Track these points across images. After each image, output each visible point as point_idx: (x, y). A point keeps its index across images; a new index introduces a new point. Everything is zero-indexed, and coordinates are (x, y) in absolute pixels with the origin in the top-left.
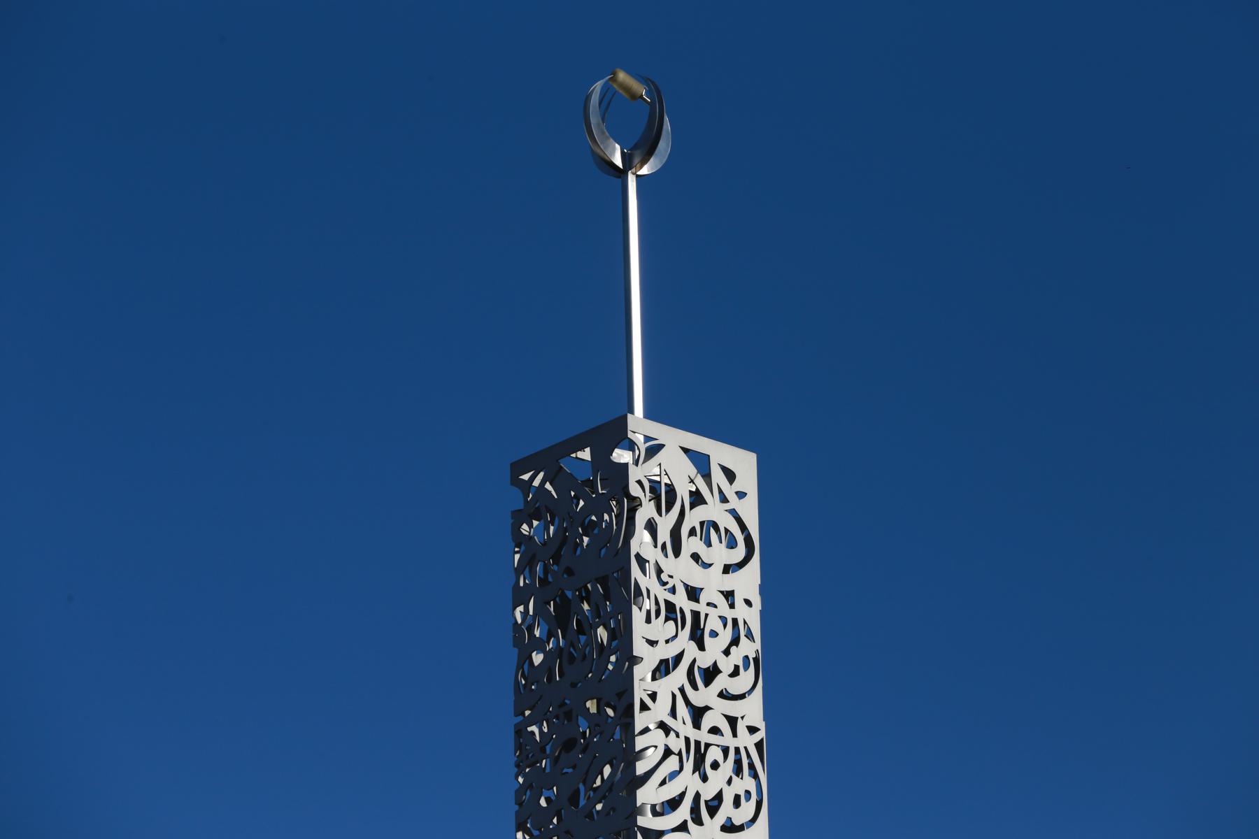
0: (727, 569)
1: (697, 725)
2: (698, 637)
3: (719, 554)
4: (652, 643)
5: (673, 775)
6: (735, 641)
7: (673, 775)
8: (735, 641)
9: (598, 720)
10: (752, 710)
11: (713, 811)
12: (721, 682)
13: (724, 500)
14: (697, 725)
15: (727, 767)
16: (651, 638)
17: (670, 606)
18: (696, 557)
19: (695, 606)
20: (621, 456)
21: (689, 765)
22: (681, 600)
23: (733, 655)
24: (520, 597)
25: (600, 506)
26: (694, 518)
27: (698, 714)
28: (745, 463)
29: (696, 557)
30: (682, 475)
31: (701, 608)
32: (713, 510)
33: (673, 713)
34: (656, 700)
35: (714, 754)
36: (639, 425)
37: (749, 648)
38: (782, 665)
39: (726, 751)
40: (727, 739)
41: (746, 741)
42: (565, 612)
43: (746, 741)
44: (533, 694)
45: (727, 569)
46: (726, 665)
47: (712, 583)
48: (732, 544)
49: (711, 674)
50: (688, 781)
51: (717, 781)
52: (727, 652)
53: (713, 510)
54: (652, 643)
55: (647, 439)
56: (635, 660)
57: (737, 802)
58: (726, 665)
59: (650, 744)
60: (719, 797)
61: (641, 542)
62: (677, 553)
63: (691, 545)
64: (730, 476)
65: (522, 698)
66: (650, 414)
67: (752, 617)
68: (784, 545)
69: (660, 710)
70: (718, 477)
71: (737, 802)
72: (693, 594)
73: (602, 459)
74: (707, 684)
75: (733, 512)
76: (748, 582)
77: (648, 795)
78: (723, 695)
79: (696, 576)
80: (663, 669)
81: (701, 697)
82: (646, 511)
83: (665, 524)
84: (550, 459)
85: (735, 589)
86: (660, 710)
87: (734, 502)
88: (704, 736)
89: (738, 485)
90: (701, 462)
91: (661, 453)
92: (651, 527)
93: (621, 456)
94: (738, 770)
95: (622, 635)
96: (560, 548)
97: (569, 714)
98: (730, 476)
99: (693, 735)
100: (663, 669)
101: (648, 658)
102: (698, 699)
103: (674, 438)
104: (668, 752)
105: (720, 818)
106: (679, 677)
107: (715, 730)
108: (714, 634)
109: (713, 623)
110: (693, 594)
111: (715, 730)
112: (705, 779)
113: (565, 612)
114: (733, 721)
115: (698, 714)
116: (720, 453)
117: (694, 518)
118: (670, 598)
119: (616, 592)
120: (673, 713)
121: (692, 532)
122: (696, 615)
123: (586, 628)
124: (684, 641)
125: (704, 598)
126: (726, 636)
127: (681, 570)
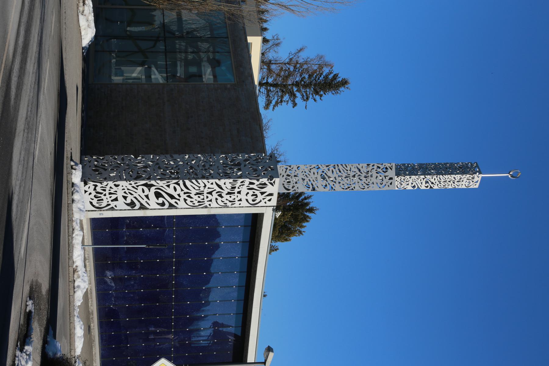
0: (247, 200)
1: (207, 193)
2: (229, 193)
3: (467, 184)
4: (225, 184)
5: (194, 188)
6: (230, 201)
7: (194, 188)
8: (230, 201)
9: (449, 171)
10: (450, 187)
11: (219, 195)
12: (219, 198)
13: (263, 199)
14: (207, 193)
15: (199, 200)
16: (458, 177)
17: (235, 188)
18: (248, 193)
19: (236, 193)
20: (478, 174)
21: (198, 191)
22: (236, 190)
23: (456, 185)
24: (462, 163)
25: (472, 171)
26: (471, 181)
27: (450, 181)
28: (477, 186)
29: (248, 193)
30: (475, 180)
31: (236, 194)
32: (260, 197)
33: (209, 188)
34: (452, 177)
35: (202, 197)
36: (481, 176)
37: (457, 187)
38: (455, 190)
39: (203, 199)
40: (206, 200)
41: (447, 186)
42: (461, 168)
43: (447, 186)
44: (452, 165)
45: (247, 200)
46: (223, 199)
47: (464, 183)
48: (253, 201)
49: (454, 183)
50: (442, 180)
51: (442, 183)
52: (227, 200)
53: (472, 183)
54: (225, 184)
55: (274, 182)
56: (219, 180)
57: (191, 202)
58: (223, 199)
59: (446, 177)
60: (191, 198)
61: (468, 176)
62: (248, 189)
63: (468, 181)
64: (270, 200)
65: (451, 163)
66: (482, 177)
67: (460, 187)
68: (468, 191)
69: (450, 178)
70: (269, 198)
71: (191, 202)
72: (239, 192)
73: (477, 172)
74: (218, 195)
75: (261, 201)
76: (464, 187)
77: (441, 176)
78: (216, 199)
79: (464, 181)
80: (455, 178)
81: (215, 195)
82: (471, 176)
83: (470, 178)
84: (477, 166)
85: (463, 185)
86: (450, 178)
87: (263, 201)
88: (205, 195)
89: (267, 202)
90: (477, 182)
91: (478, 178)
92: (253, 184)
93: (478, 174)
94: (199, 202)
95: (458, 174)
96: (468, 168)
97: (450, 168)
98: (270, 200)
99: (205, 192)
100: (455, 178)
101: (456, 176)
102: (214, 193)
103: (480, 179)
104: (199, 187)
105: (187, 198)
106: (218, 189)
107: (207, 197)
108: (230, 197)
109: (233, 197)
110: (239, 192)
111: (207, 197)
112: (195, 195)
113: (461, 168)
114: (211, 201)
115: (450, 181)
116: (478, 184)
117: (471, 181)
118: (237, 188)
119: (463, 173)
120: (209, 188)
121: (254, 192)
122: (234, 193)
123: (459, 170)
124: (227, 191)
125: (238, 195)
126: (231, 199)
127: (465, 180)
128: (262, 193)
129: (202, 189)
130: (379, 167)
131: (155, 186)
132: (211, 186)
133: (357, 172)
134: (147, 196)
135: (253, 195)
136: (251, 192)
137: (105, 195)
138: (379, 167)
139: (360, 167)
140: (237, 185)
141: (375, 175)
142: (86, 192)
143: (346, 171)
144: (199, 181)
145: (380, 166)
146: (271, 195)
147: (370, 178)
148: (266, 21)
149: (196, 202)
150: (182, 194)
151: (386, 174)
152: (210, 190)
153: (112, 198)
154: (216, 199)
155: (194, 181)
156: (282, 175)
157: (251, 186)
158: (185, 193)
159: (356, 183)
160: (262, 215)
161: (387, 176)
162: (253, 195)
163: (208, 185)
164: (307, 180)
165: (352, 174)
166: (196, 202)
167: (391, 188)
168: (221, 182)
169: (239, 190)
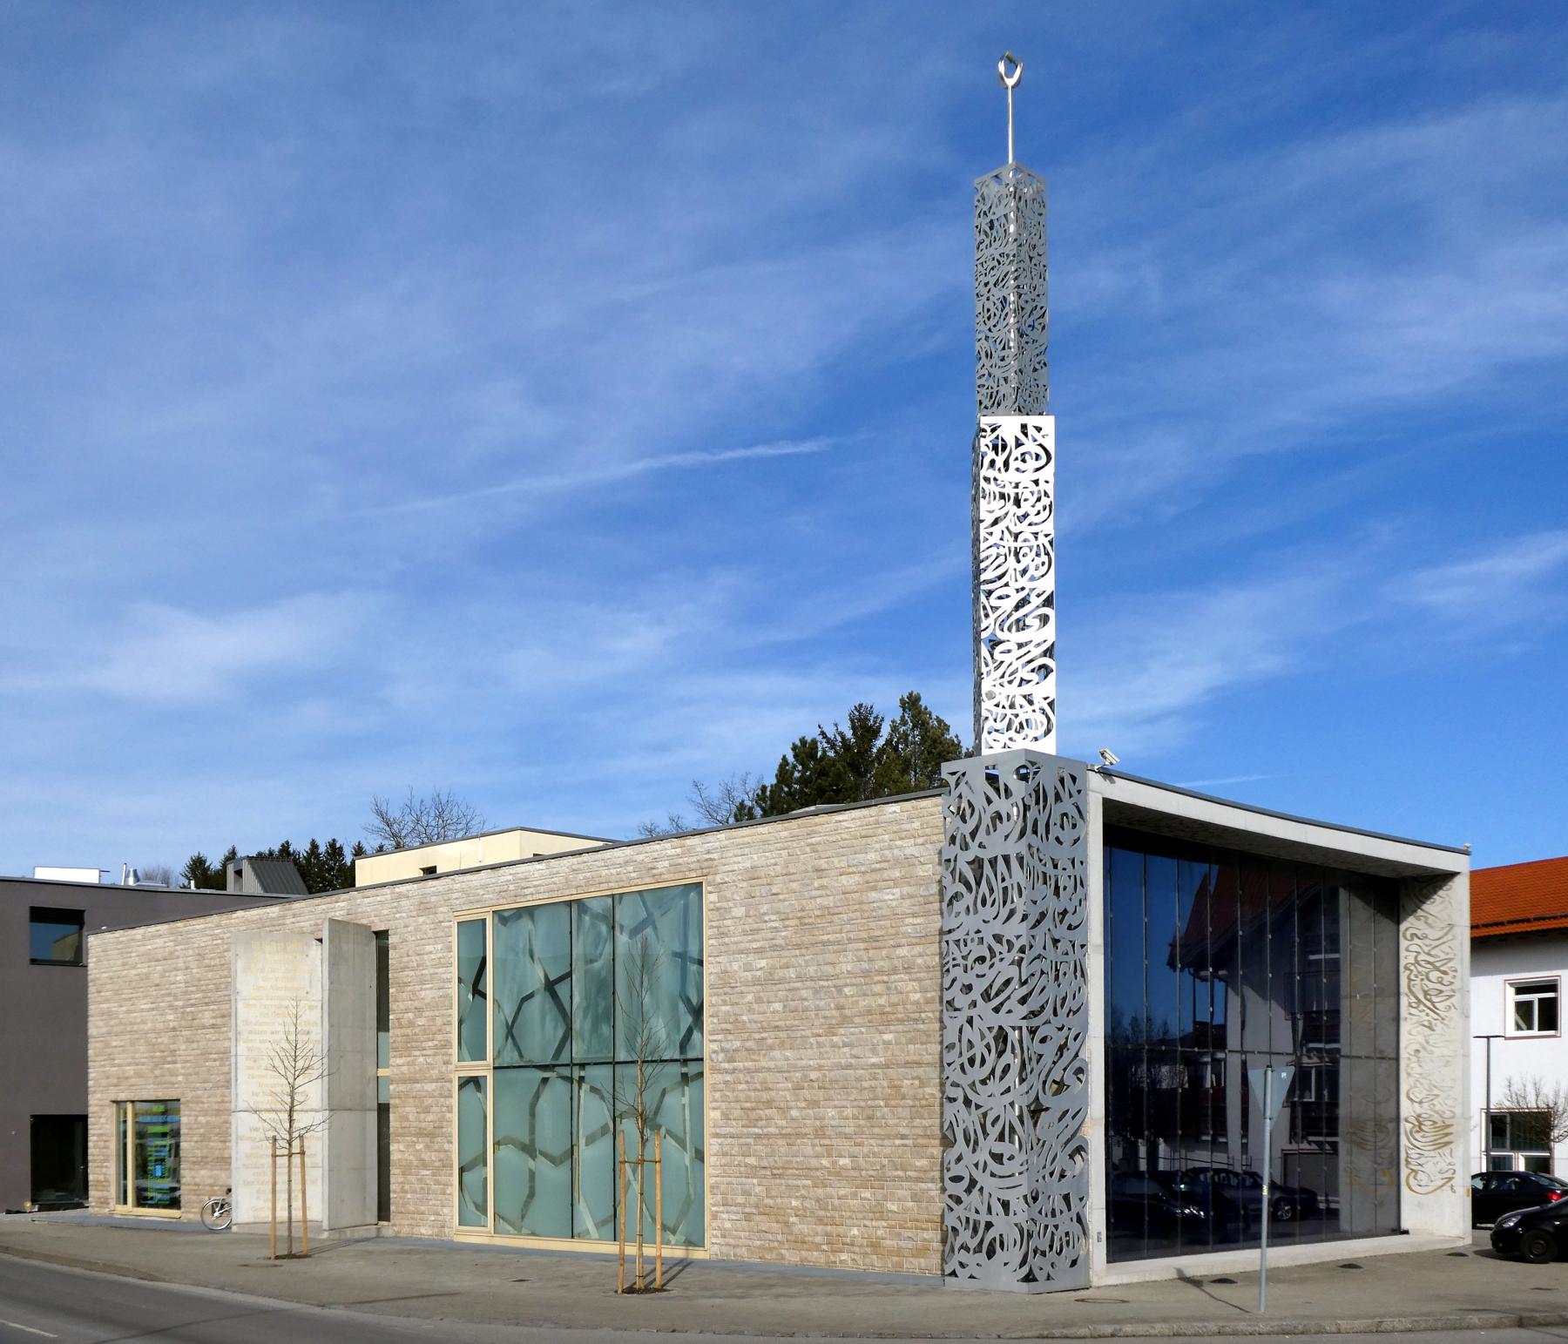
2: (1017, 503)
18: (1057, 839)
29: (1057, 839)
58: (1033, 512)
64: (1039, 429)
94: (1038, 555)
106: (1047, 923)
126: (1070, 889)
128: (1058, 798)
129: (1045, 965)
130: (992, 463)
131: (1037, 1098)
132: (997, 535)
133: (1001, 526)
134: (1020, 646)
135: (1024, 461)
136: (1055, 831)
137: (1056, 1227)
138: (992, 463)
139: (989, 519)
140: (1040, 868)
141: (1011, 475)
142: (1049, 1277)
143: (1002, 559)
144: (982, 556)
145: (986, 462)
146: (1024, 427)
147: (1019, 491)
148: (314, 846)
149: (1038, 561)
150: (1056, 1022)
151: (1011, 443)
152: (1049, 944)
153: (1065, 1208)
154: (1070, 927)
155: (983, 566)
156: (1009, 743)
157: (1041, 829)
158: (1055, 1014)
159: (1034, 529)
160: (1110, 806)
161: (1017, 439)
162: (1024, 461)
163: (992, 540)
164: (1024, 673)
165: (1009, 542)
166: (1038, 561)
167: (1051, 493)
168: (988, 519)
169: (1050, 864)
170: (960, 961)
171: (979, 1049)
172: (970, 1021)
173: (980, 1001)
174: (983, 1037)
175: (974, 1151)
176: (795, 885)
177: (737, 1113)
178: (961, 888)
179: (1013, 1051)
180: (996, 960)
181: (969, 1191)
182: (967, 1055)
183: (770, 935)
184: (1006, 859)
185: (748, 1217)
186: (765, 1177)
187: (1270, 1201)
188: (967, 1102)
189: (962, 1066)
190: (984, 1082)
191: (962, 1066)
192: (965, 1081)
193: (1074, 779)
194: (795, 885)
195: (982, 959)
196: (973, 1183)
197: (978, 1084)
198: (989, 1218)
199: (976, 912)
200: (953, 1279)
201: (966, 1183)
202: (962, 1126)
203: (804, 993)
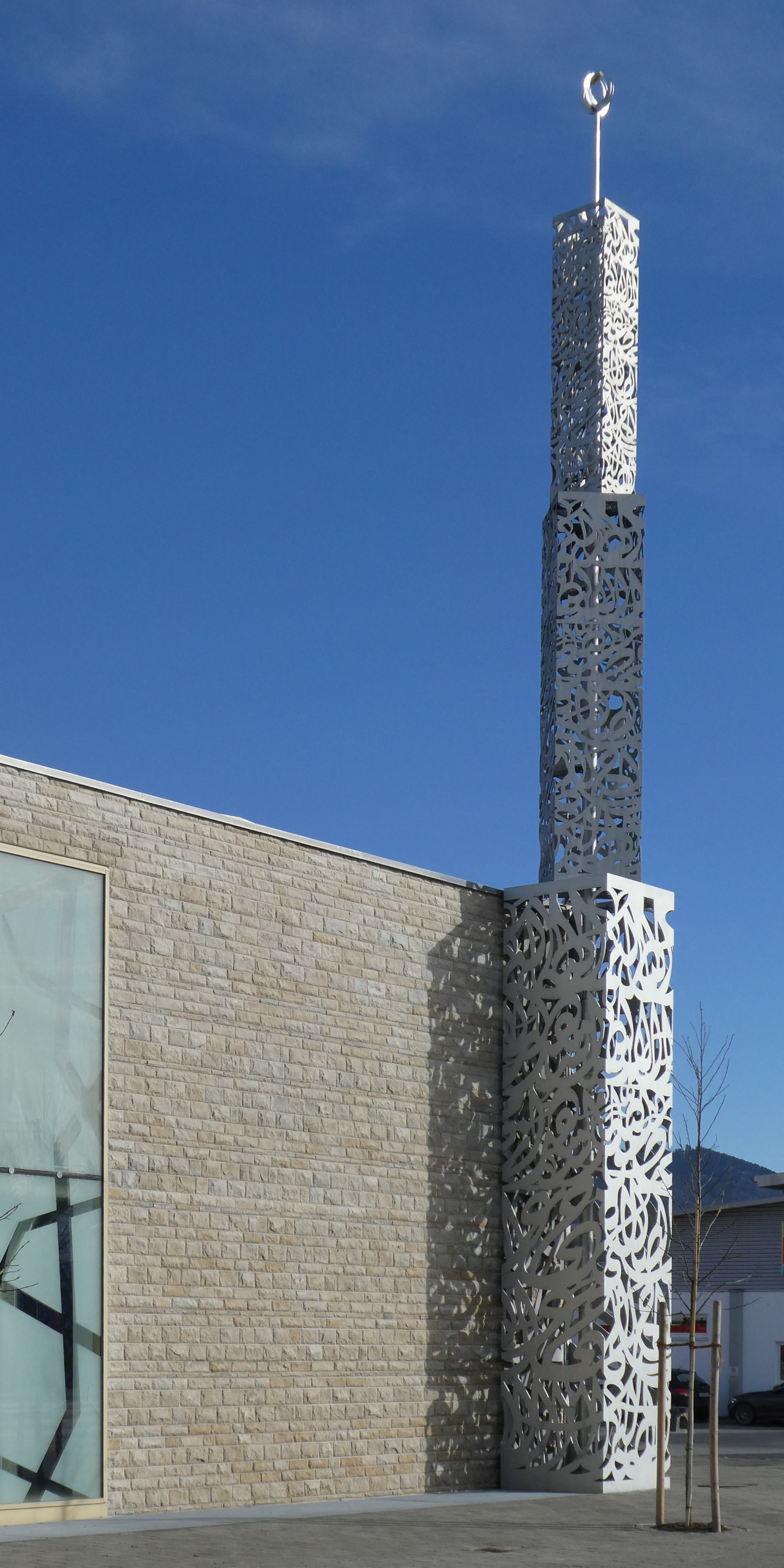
170: (619, 1112)
171: (635, 1218)
172: (627, 1182)
173: (635, 1163)
174: (638, 1204)
175: (629, 1335)
176: (252, 933)
177: (158, 1273)
178: (579, 589)
179: (662, 1224)
180: (649, 1118)
181: (624, 1380)
182: (625, 1223)
183: (212, 998)
184: (624, 571)
185: (172, 1441)
186: (200, 1374)
187: (695, 1435)
188: (624, 1277)
189: (620, 1235)
190: (639, 1255)
191: (620, 1235)
192: (623, 1253)
193: (569, 853)
194: (252, 933)
195: (636, 1116)
196: (629, 1369)
197: (634, 1258)
198: (641, 1409)
199: (633, 1060)
200: (609, 1483)
201: (622, 1371)
202: (620, 1305)
203: (263, 1098)
